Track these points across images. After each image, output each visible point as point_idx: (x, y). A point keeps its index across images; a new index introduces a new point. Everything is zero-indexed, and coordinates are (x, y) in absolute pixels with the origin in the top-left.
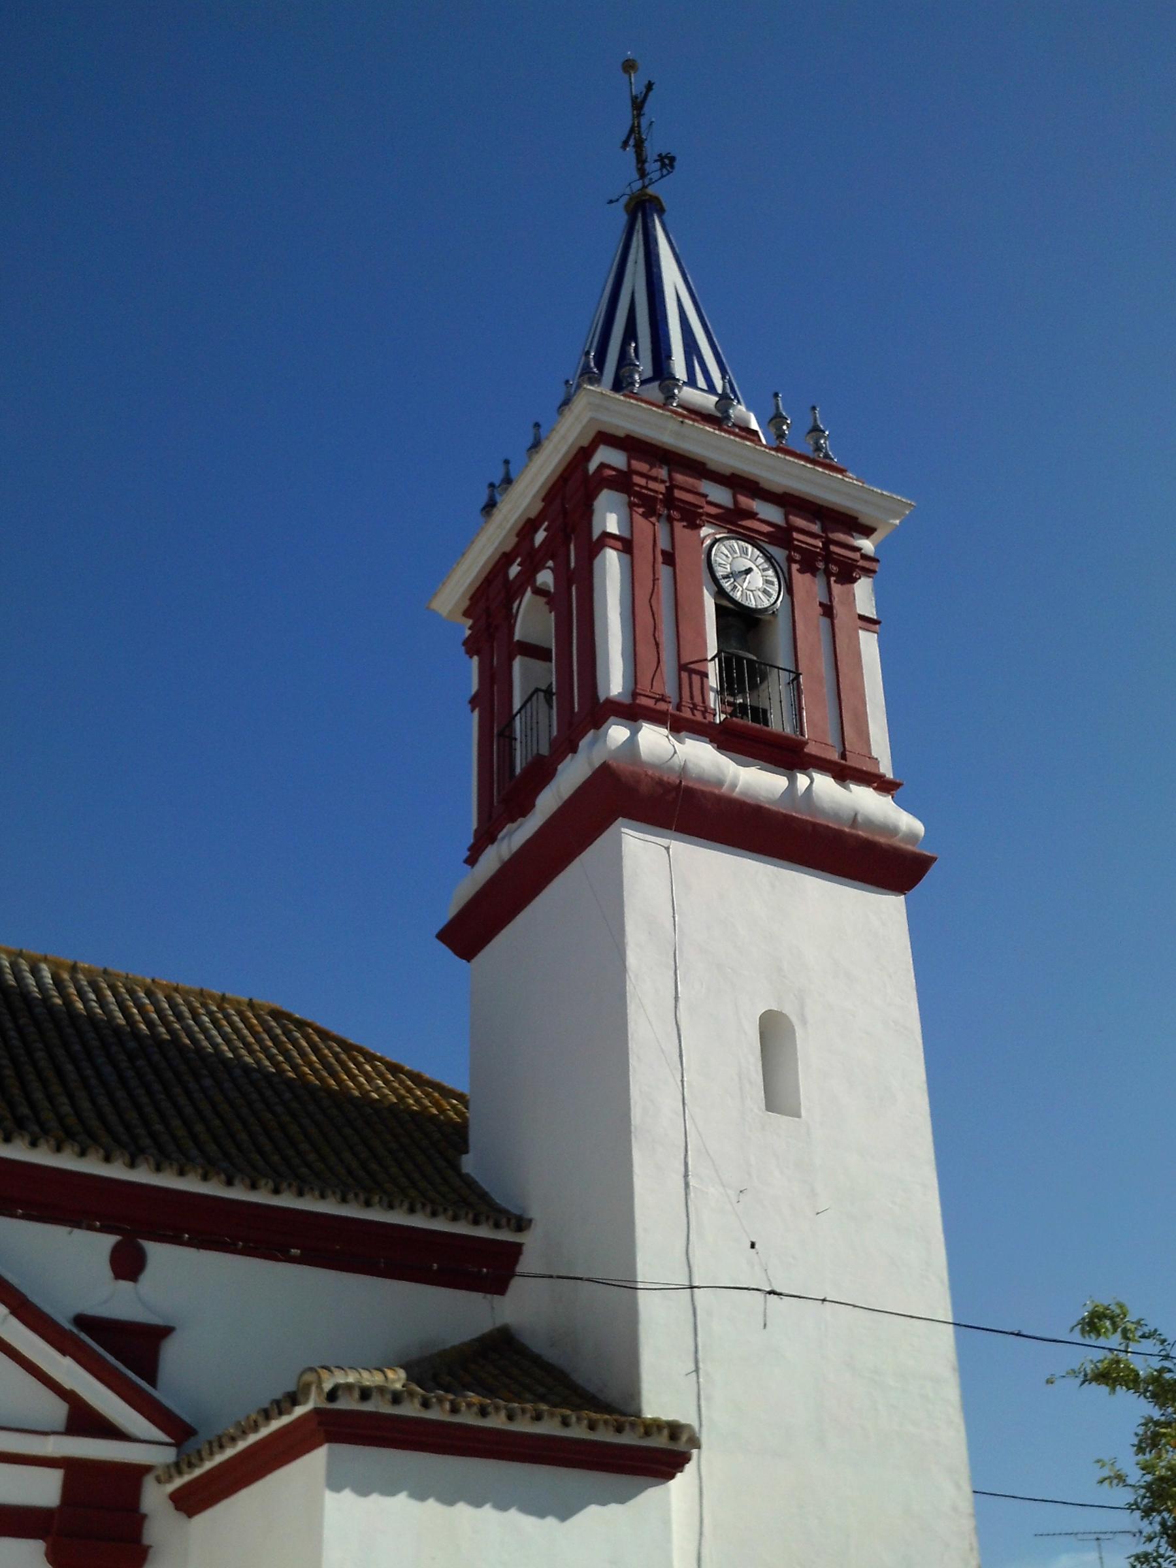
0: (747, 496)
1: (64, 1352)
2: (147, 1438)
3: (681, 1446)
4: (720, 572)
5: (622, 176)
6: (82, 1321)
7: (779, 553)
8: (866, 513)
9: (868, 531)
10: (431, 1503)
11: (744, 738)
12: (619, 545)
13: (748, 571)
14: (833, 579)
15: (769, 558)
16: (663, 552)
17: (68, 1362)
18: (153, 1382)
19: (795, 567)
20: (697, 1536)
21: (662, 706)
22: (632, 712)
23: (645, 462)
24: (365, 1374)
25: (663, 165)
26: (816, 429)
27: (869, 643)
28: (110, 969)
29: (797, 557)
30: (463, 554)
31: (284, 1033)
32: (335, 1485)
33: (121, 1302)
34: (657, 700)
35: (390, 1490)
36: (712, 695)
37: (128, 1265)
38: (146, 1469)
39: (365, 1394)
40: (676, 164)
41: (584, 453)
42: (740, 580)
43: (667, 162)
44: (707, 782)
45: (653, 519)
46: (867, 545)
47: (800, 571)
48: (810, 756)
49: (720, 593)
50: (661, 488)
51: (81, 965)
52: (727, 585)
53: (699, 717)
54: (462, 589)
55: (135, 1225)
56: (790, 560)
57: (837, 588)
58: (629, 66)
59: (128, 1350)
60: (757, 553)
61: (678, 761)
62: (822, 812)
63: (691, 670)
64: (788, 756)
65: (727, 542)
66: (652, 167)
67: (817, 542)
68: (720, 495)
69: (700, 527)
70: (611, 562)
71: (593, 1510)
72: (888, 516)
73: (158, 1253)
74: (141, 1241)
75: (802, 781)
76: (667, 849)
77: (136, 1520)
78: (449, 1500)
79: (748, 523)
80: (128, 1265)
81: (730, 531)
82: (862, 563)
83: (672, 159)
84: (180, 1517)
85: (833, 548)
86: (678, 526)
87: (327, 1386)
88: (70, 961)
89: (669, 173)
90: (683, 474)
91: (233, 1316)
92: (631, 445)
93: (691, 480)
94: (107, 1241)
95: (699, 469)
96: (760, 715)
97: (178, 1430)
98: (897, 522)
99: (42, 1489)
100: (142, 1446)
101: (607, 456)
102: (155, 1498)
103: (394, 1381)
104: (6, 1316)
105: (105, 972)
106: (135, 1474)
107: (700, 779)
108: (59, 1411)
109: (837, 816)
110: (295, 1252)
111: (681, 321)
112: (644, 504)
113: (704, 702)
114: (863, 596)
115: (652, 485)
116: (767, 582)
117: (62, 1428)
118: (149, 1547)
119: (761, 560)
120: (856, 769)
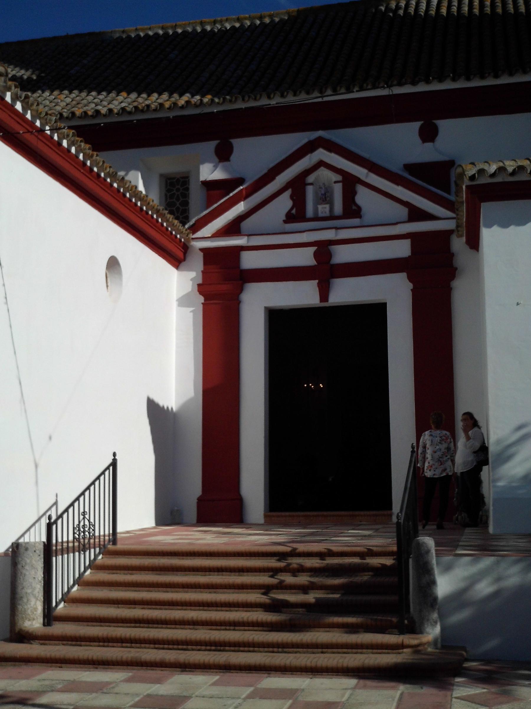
1: (398, 184)
2: (446, 217)
6: (408, 167)
10: (512, 227)
17: (400, 188)
33: (425, 153)
37: (429, 134)
38: (451, 232)
55: (427, 114)
74: (435, 121)
77: (450, 256)
80: (429, 134)
94: (416, 125)
99: (402, 249)
104: (367, 173)
106: (446, 235)
108: (404, 212)
110: (294, 211)
117: (407, 219)
118: (456, 269)
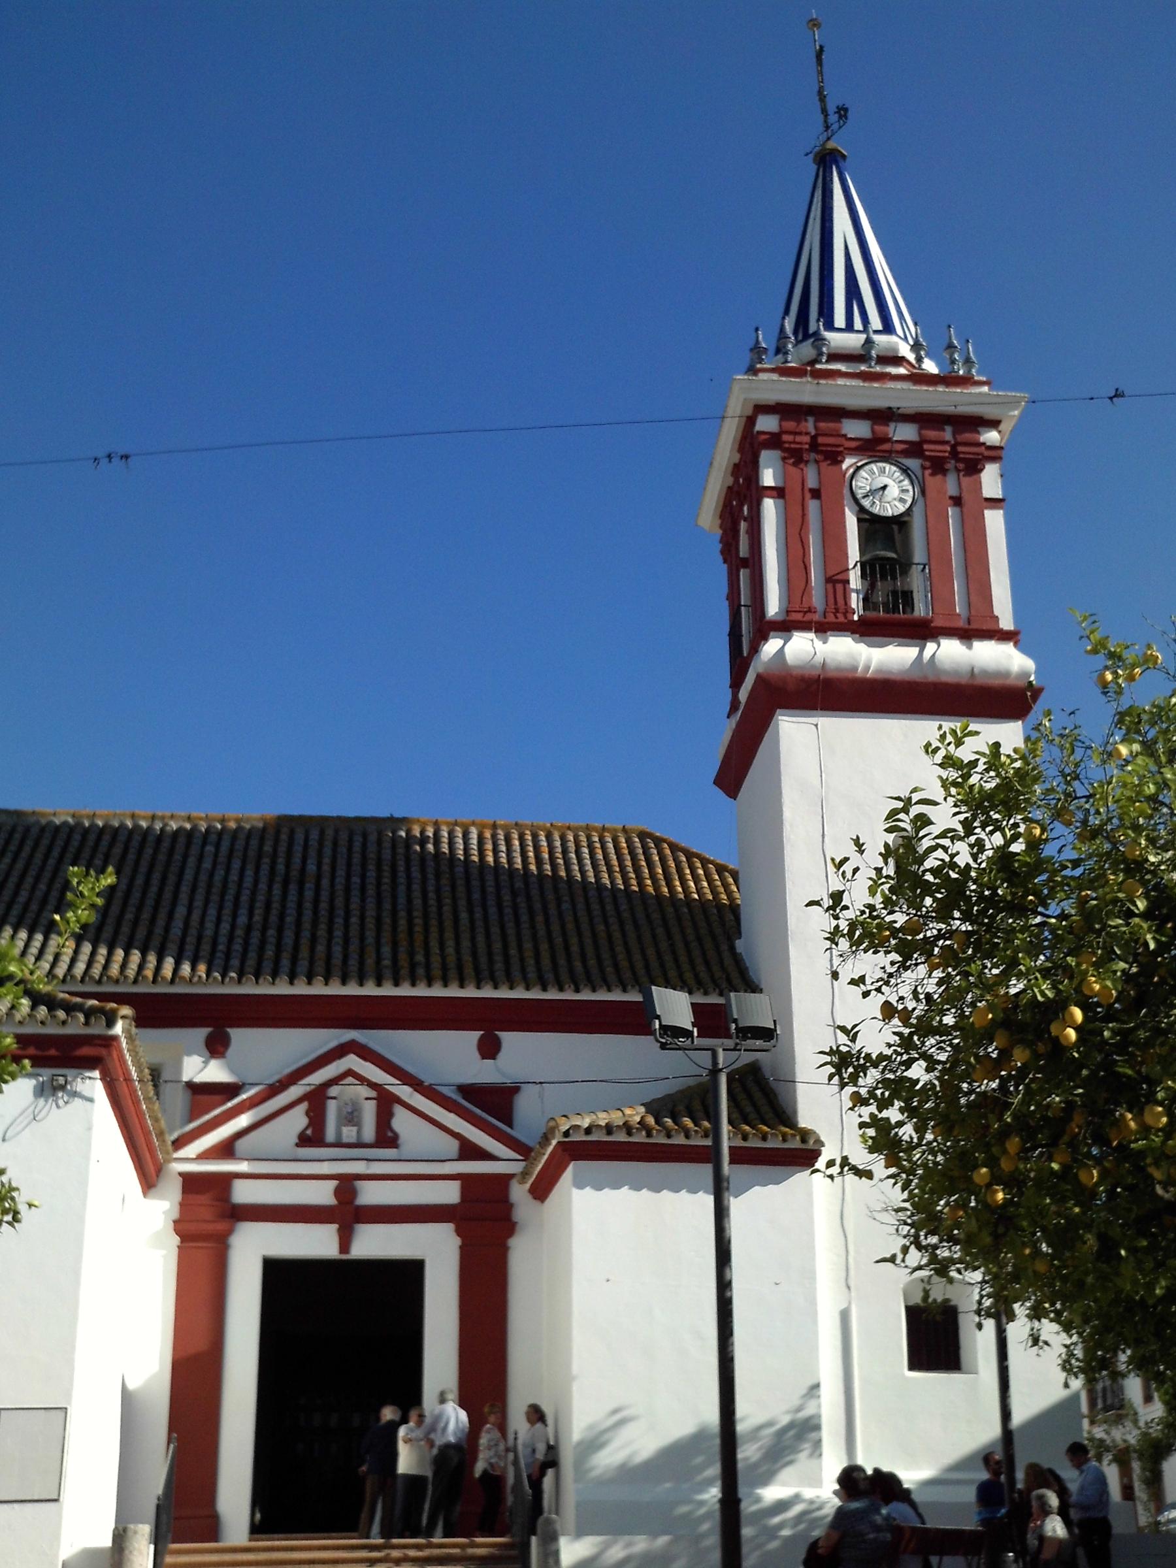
0: (881, 424)
3: (811, 1144)
4: (860, 493)
5: (811, 136)
7: (913, 463)
8: (989, 412)
9: (994, 424)
11: (889, 621)
12: (775, 493)
13: (884, 488)
14: (961, 474)
15: (905, 471)
16: (811, 490)
17: (452, 1116)
18: (510, 1125)
19: (928, 472)
20: (840, 1202)
21: (809, 617)
22: (785, 627)
23: (792, 420)
24: (602, 1115)
25: (840, 117)
26: (951, 347)
27: (995, 521)
28: (520, 822)
29: (928, 464)
30: (705, 489)
31: (644, 853)
32: (580, 1186)
33: (485, 1073)
34: (805, 613)
35: (616, 1186)
36: (854, 596)
37: (489, 1049)
38: (511, 1176)
39: (609, 1129)
40: (849, 114)
41: (751, 421)
42: (877, 497)
43: (843, 112)
44: (846, 670)
45: (802, 466)
46: (991, 437)
47: (932, 475)
48: (936, 628)
49: (862, 510)
50: (807, 439)
51: (498, 822)
52: (866, 503)
53: (841, 619)
54: (712, 512)
55: (490, 1024)
56: (924, 468)
57: (966, 481)
58: (814, 23)
59: (492, 1103)
60: (894, 468)
61: (819, 659)
62: (945, 672)
63: (836, 581)
64: (921, 632)
65: (867, 467)
66: (833, 118)
67: (947, 447)
68: (856, 429)
69: (842, 462)
70: (769, 506)
71: (757, 1188)
72: (1006, 411)
73: (508, 1038)
75: (930, 647)
76: (816, 725)
78: (657, 1189)
79: (886, 446)
80: (489, 1049)
81: (871, 457)
82: (987, 453)
83: (846, 110)
84: (537, 1203)
85: (960, 449)
86: (824, 465)
87: (564, 1128)
88: (491, 821)
89: (845, 123)
90: (824, 421)
91: (567, 1074)
92: (784, 410)
93: (831, 425)
95: (839, 413)
96: (907, 598)
97: (524, 1151)
98: (1016, 413)
99: (449, 1193)
100: (504, 1162)
101: (767, 424)
102: (519, 1193)
103: (630, 1116)
105: (516, 824)
106: (504, 1180)
107: (838, 669)
108: (453, 1146)
109: (956, 672)
111: (846, 272)
112: (794, 457)
113: (846, 604)
114: (991, 481)
115: (798, 439)
116: (904, 491)
119: (897, 474)
120: (977, 630)
